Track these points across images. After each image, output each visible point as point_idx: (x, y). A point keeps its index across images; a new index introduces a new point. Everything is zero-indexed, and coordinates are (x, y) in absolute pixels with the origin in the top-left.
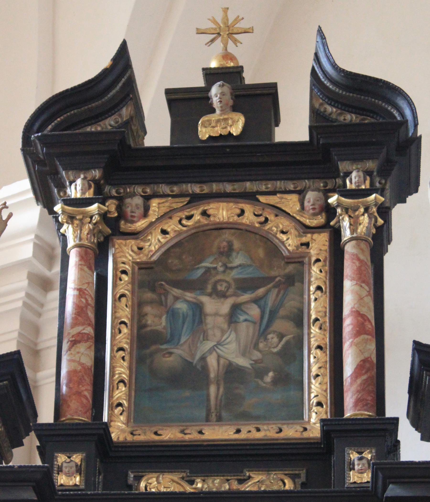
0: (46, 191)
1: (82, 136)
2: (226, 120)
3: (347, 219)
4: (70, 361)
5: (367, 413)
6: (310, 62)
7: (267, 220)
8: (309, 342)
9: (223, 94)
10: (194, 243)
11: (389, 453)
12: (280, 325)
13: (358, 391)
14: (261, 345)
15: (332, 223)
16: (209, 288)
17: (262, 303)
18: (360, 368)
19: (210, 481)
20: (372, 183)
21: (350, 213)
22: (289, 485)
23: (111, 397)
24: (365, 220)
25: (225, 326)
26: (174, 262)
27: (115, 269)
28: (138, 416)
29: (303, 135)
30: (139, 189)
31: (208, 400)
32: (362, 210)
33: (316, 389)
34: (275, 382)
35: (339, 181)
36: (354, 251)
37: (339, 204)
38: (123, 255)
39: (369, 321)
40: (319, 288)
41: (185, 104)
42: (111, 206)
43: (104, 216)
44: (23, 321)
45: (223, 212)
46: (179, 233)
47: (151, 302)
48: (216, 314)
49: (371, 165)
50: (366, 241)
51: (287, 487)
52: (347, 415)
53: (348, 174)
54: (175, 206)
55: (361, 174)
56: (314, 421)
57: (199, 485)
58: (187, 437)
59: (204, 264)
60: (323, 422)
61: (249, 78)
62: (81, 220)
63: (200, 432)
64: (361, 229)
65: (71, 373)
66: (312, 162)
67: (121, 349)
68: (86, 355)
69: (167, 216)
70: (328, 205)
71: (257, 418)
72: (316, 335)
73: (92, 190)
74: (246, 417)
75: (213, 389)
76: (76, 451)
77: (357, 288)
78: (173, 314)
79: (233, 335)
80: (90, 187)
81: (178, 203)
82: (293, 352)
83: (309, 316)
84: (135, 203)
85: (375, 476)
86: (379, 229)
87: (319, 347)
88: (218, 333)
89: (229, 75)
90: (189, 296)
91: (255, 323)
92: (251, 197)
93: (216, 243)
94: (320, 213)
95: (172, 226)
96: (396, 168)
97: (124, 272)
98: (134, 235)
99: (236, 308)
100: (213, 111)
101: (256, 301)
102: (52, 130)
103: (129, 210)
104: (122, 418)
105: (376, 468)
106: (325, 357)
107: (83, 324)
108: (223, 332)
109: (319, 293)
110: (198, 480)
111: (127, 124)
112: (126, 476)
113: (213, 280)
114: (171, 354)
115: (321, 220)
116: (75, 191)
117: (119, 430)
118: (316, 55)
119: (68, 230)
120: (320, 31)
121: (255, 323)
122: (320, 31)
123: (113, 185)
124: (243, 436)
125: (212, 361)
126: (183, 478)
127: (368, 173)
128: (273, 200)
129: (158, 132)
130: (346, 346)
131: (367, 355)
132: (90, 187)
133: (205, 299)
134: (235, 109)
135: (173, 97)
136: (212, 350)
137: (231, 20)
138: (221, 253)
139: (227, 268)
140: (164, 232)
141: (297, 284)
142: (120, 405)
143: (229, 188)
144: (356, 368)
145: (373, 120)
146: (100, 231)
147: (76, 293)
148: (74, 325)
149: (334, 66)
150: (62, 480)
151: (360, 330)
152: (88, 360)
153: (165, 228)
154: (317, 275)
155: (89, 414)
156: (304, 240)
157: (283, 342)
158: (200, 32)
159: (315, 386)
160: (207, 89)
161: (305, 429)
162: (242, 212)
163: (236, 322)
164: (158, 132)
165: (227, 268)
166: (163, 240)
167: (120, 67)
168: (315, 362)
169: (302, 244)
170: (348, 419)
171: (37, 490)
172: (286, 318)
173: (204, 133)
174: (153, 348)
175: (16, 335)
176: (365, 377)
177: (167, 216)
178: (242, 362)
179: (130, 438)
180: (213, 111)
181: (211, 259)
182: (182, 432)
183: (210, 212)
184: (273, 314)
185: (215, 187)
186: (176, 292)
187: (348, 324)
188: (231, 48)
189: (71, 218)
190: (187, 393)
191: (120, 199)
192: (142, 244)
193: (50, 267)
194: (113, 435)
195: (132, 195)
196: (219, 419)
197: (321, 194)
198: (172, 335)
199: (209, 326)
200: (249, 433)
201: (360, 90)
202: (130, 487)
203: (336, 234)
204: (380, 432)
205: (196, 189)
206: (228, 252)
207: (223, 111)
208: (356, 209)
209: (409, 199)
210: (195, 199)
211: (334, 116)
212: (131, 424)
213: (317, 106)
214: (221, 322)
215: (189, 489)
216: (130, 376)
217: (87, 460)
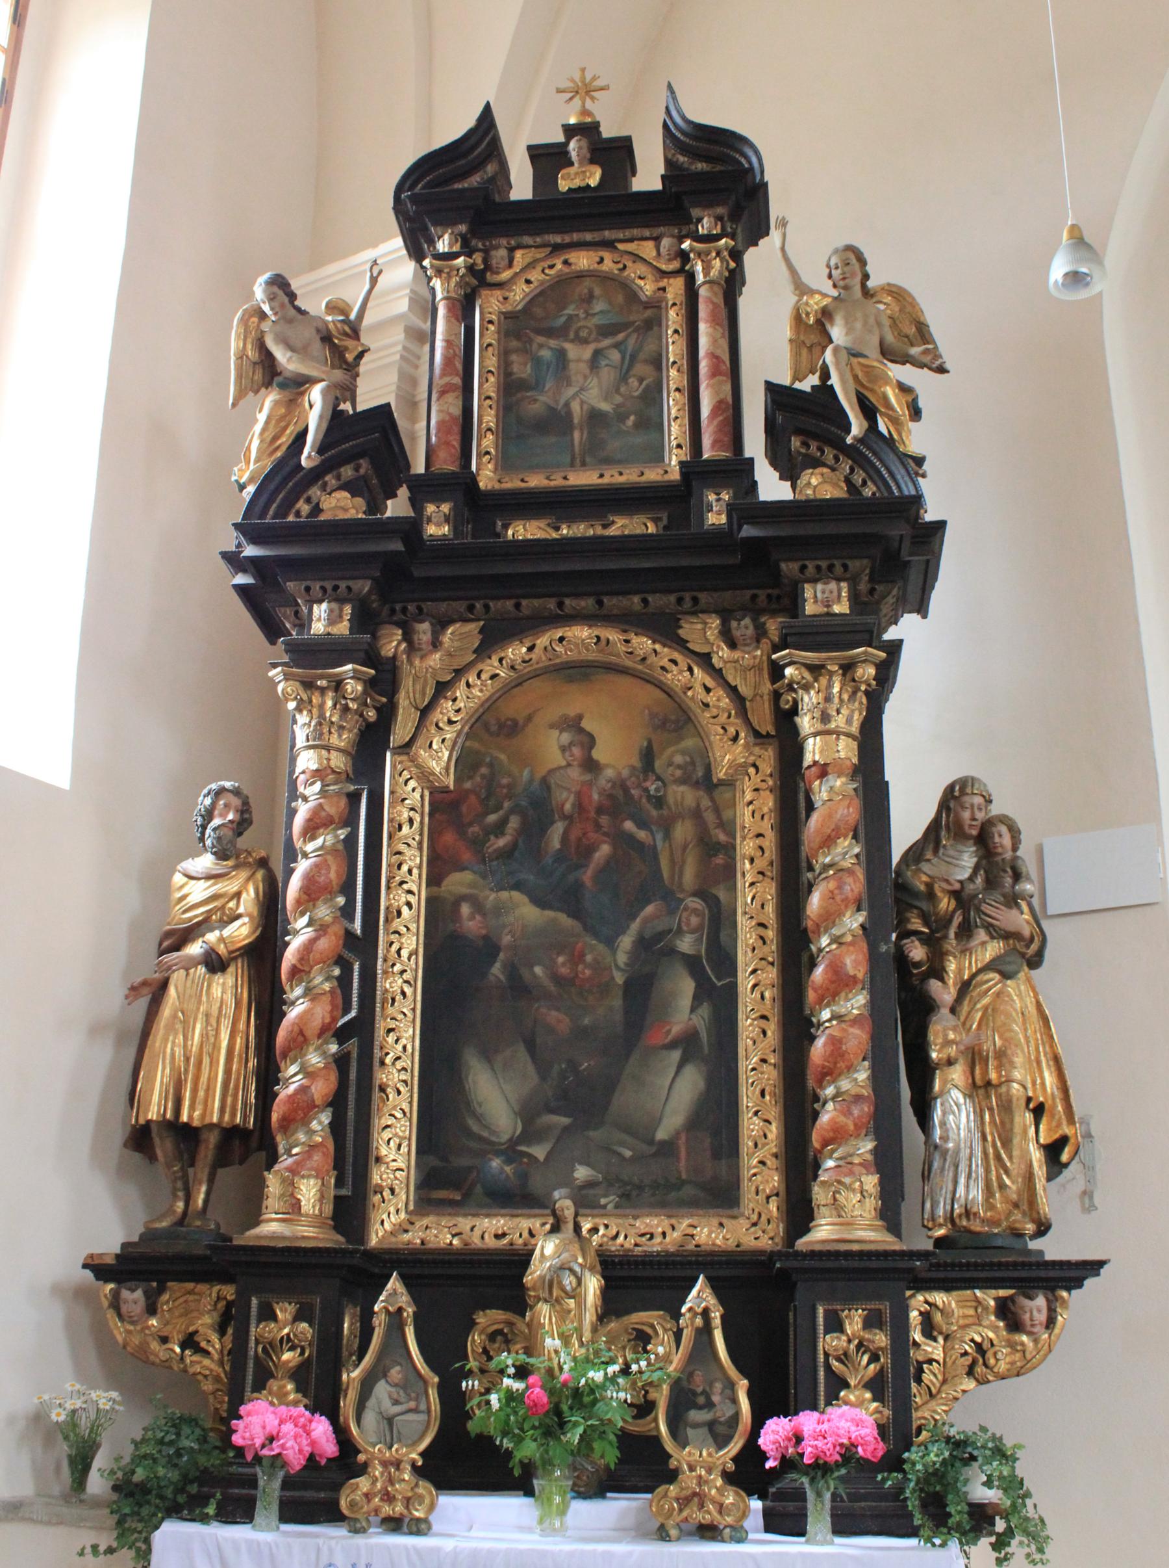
0: (416, 248)
1: (450, 193)
2: (584, 172)
3: (699, 263)
4: (439, 411)
5: (725, 454)
6: (662, 116)
7: (625, 267)
8: (668, 385)
9: (580, 148)
10: (557, 291)
11: (747, 493)
12: (640, 369)
13: (715, 432)
14: (622, 389)
15: (687, 268)
16: (572, 335)
17: (623, 347)
18: (717, 409)
19: (574, 527)
20: (723, 228)
21: (703, 257)
22: (652, 529)
23: (479, 445)
24: (717, 263)
25: (587, 371)
26: (538, 311)
27: (482, 319)
28: (505, 463)
29: (658, 186)
30: (504, 241)
31: (573, 445)
32: (714, 254)
33: (675, 431)
34: (637, 425)
35: (692, 227)
36: (708, 294)
37: (692, 249)
38: (489, 305)
39: (724, 363)
40: (676, 331)
41: (547, 159)
42: (478, 258)
43: (471, 269)
44: (402, 375)
45: (583, 260)
46: (542, 283)
47: (516, 351)
48: (579, 360)
49: (720, 210)
50: (719, 284)
51: (650, 531)
52: (705, 456)
53: (700, 220)
54: (538, 256)
55: (712, 220)
56: (674, 460)
57: (565, 532)
58: (552, 484)
59: (566, 312)
60: (681, 463)
61: (607, 132)
62: (448, 273)
63: (565, 478)
64: (714, 273)
65: (440, 424)
66: (668, 209)
67: (489, 398)
68: (454, 405)
69: (530, 266)
70: (682, 250)
71: (620, 462)
72: (675, 377)
73: (459, 244)
74: (608, 461)
75: (576, 435)
76: (444, 501)
77: (710, 330)
78: (537, 362)
79: (595, 381)
80: (457, 241)
81: (540, 254)
82: (653, 395)
83: (668, 359)
84: (499, 255)
85: (729, 517)
86: (732, 272)
87: (678, 390)
88: (581, 379)
89: (587, 130)
90: (553, 343)
91: (615, 367)
92: (609, 245)
93: (578, 290)
94: (675, 259)
95: (535, 276)
96: (746, 212)
97: (490, 322)
98: (500, 285)
99: (597, 353)
100: (572, 164)
101: (616, 346)
102: (424, 188)
103: (494, 262)
104: (490, 466)
105: (731, 509)
106: (683, 399)
107: (451, 375)
108: (586, 377)
109: (676, 336)
110: (564, 526)
111: (492, 180)
112: (495, 524)
113: (574, 327)
114: (536, 400)
115: (675, 265)
116: (443, 246)
117: (487, 477)
118: (667, 108)
119: (437, 283)
120: (670, 86)
121: (615, 367)
122: (670, 86)
123: (481, 238)
124: (606, 480)
125: (575, 407)
126: (549, 525)
127: (719, 218)
128: (630, 247)
129: (522, 186)
130: (703, 387)
131: (722, 396)
132: (457, 241)
133: (568, 346)
134: (592, 161)
135: (536, 152)
136: (574, 397)
137: (588, 80)
138: (583, 300)
139: (588, 315)
140: (528, 282)
141: (655, 328)
142: (488, 453)
143: (588, 237)
144: (712, 410)
145: (722, 168)
146: (467, 284)
147: (444, 344)
148: (443, 375)
149: (684, 118)
150: (431, 530)
151: (715, 372)
152: (456, 410)
153: (529, 277)
154: (674, 318)
155: (457, 463)
156: (661, 284)
157: (643, 386)
158: (559, 91)
159: (675, 428)
160: (566, 144)
161: (666, 472)
162: (602, 260)
163: (597, 367)
164: (522, 185)
165: (588, 315)
166: (527, 290)
167: (485, 125)
168: (673, 404)
169: (659, 289)
170: (706, 461)
171: (406, 541)
172: (646, 361)
173: (563, 185)
174: (519, 395)
175: (394, 387)
176: (721, 418)
177: (530, 266)
178: (605, 406)
179: (497, 486)
180: (572, 164)
181: (573, 306)
182: (548, 478)
183: (572, 260)
184: (633, 358)
185: (576, 237)
186: (540, 339)
187: (704, 366)
188: (589, 104)
189: (439, 272)
190: (553, 439)
191: (486, 252)
192: (507, 294)
193: (425, 322)
194: (481, 484)
195: (497, 247)
196: (583, 464)
197: (675, 240)
198: (537, 380)
199: (572, 372)
200: (613, 477)
201: (709, 141)
202: (498, 535)
203: (691, 277)
204: (737, 471)
205: (557, 239)
206: (590, 298)
207: (581, 164)
208: (708, 254)
209: (761, 242)
210: (557, 248)
211: (686, 166)
212: (499, 472)
213: (670, 156)
214: (584, 367)
215: (555, 535)
216: (497, 426)
217: (454, 509)
